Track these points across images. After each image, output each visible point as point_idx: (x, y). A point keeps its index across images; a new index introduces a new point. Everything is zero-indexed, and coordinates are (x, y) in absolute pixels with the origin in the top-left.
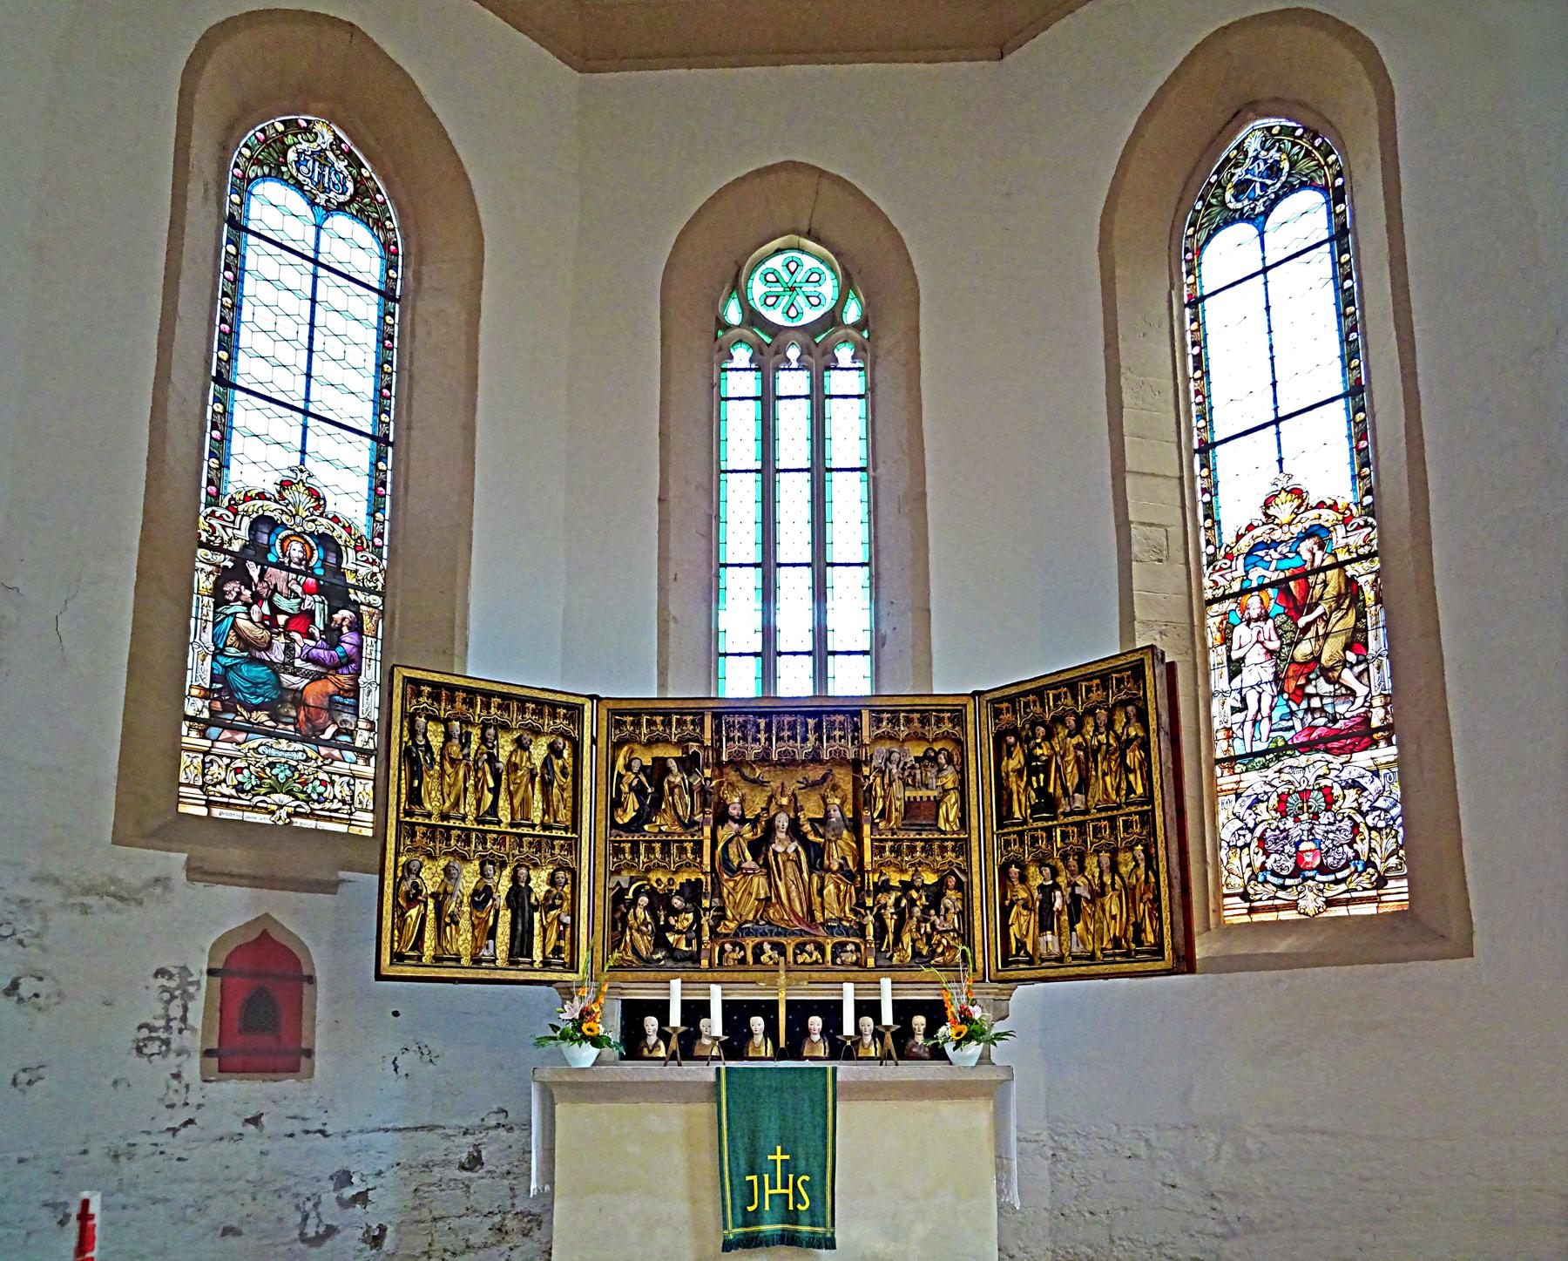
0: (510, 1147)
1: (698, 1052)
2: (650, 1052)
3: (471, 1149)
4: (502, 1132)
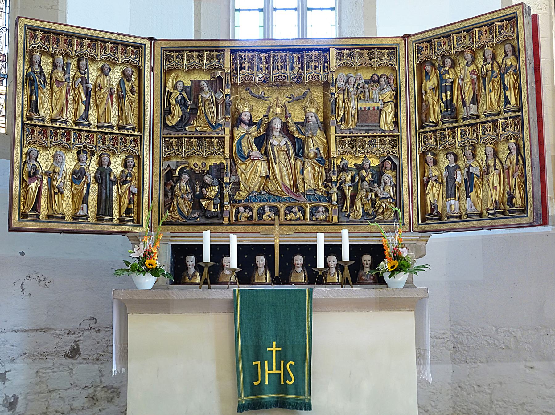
0: (98, 343)
2: (190, 279)
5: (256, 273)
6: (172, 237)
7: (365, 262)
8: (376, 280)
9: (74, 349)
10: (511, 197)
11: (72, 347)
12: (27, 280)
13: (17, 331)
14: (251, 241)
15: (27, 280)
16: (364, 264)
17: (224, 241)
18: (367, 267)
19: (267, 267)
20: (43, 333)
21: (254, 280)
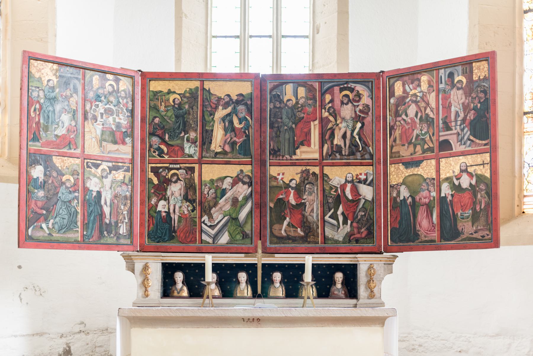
0: (87, 344)
1: (271, 294)
2: (178, 293)
3: (65, 346)
4: (83, 335)
5: (238, 288)
6: (162, 256)
7: (337, 279)
8: (347, 294)
9: (66, 350)
10: (236, 240)
11: (65, 349)
12: (24, 290)
13: (16, 336)
14: (234, 260)
15: (24, 290)
16: (336, 280)
17: (325, 261)
18: (339, 283)
19: (248, 282)
20: (39, 336)
21: (236, 294)
